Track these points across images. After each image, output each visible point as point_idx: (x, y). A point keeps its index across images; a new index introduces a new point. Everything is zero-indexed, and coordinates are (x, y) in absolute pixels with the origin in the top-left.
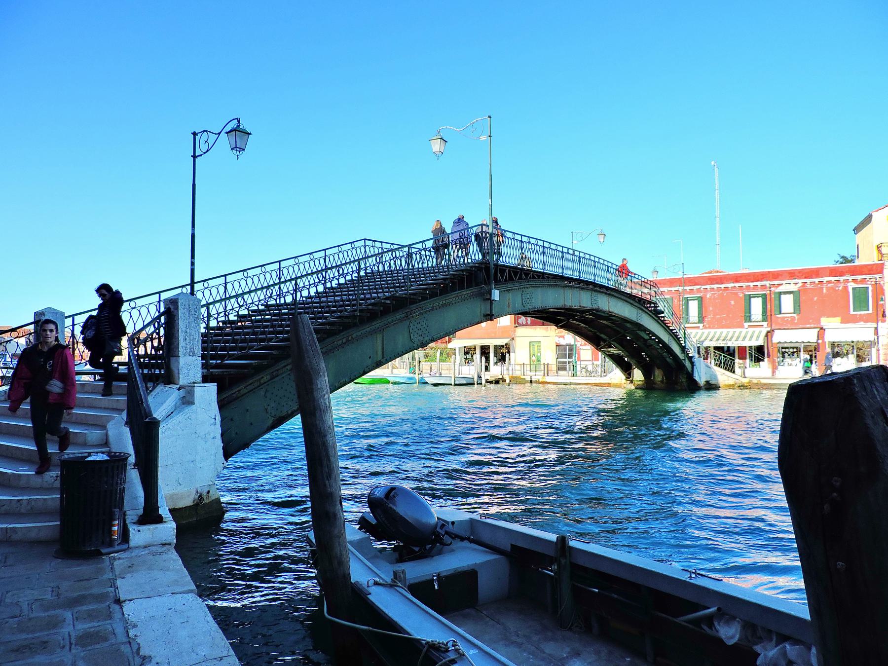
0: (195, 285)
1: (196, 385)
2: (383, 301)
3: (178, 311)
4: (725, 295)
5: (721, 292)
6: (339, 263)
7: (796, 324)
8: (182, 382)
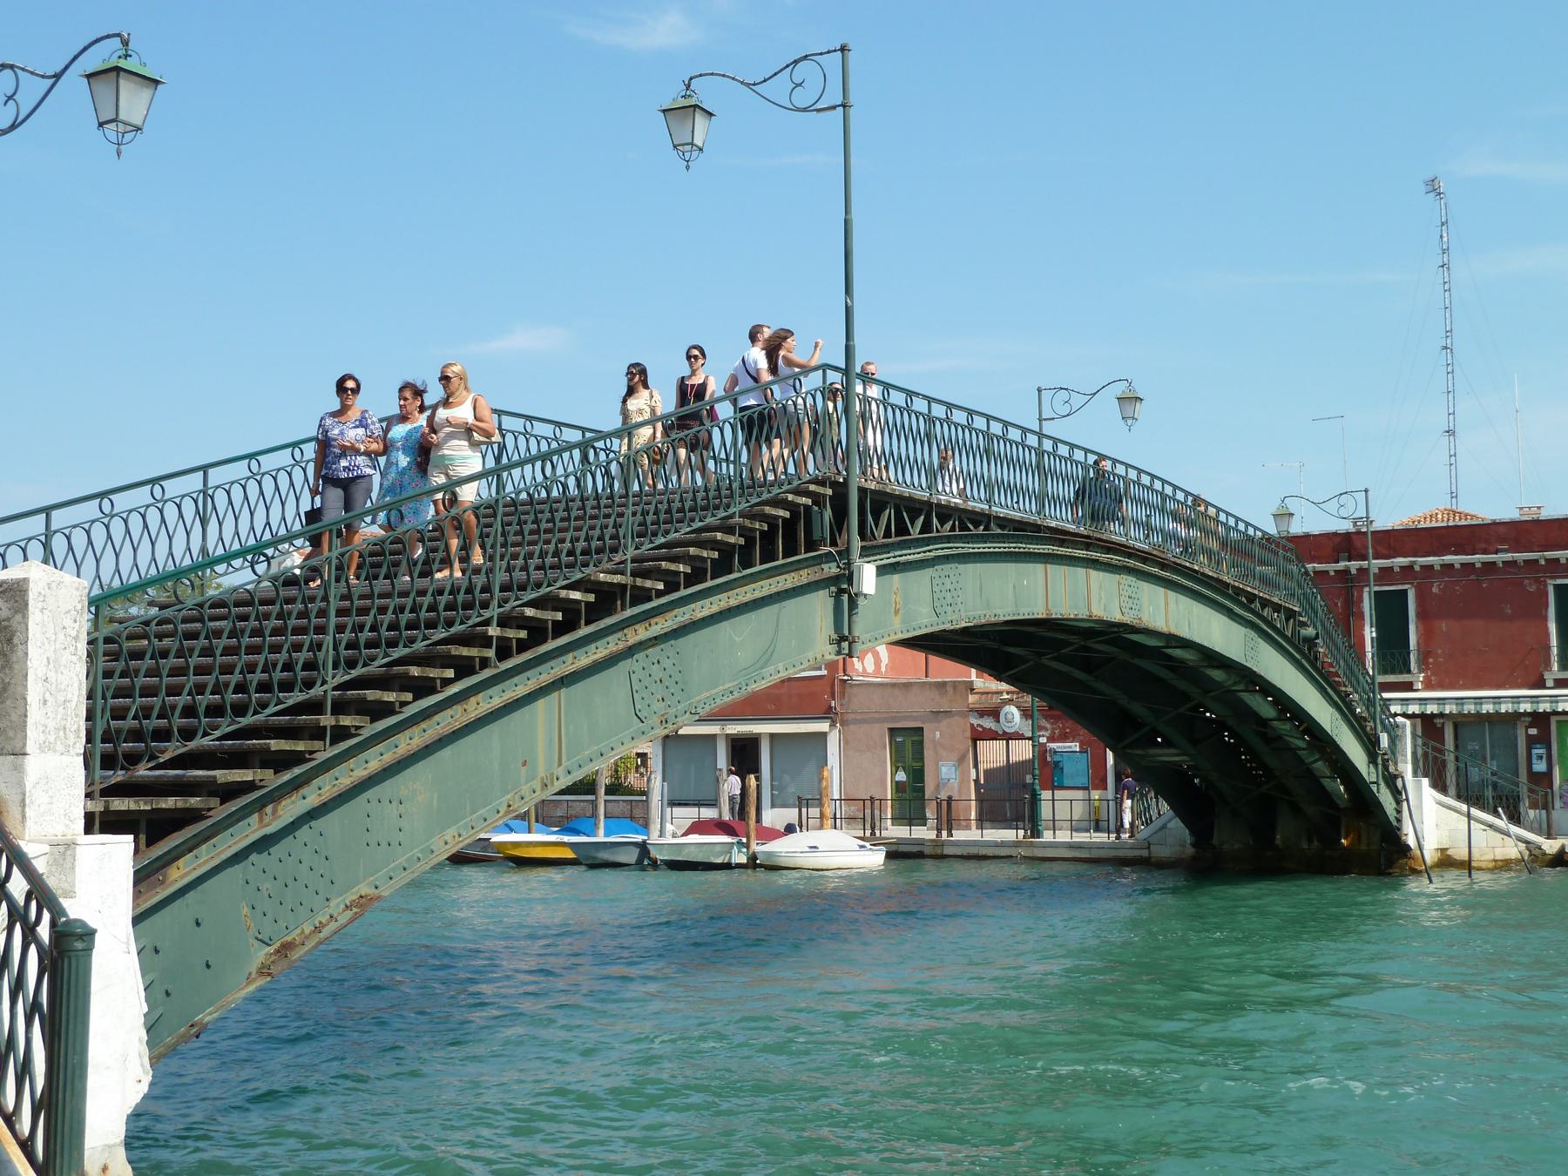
3: (25, 617)
5: (1473, 577)
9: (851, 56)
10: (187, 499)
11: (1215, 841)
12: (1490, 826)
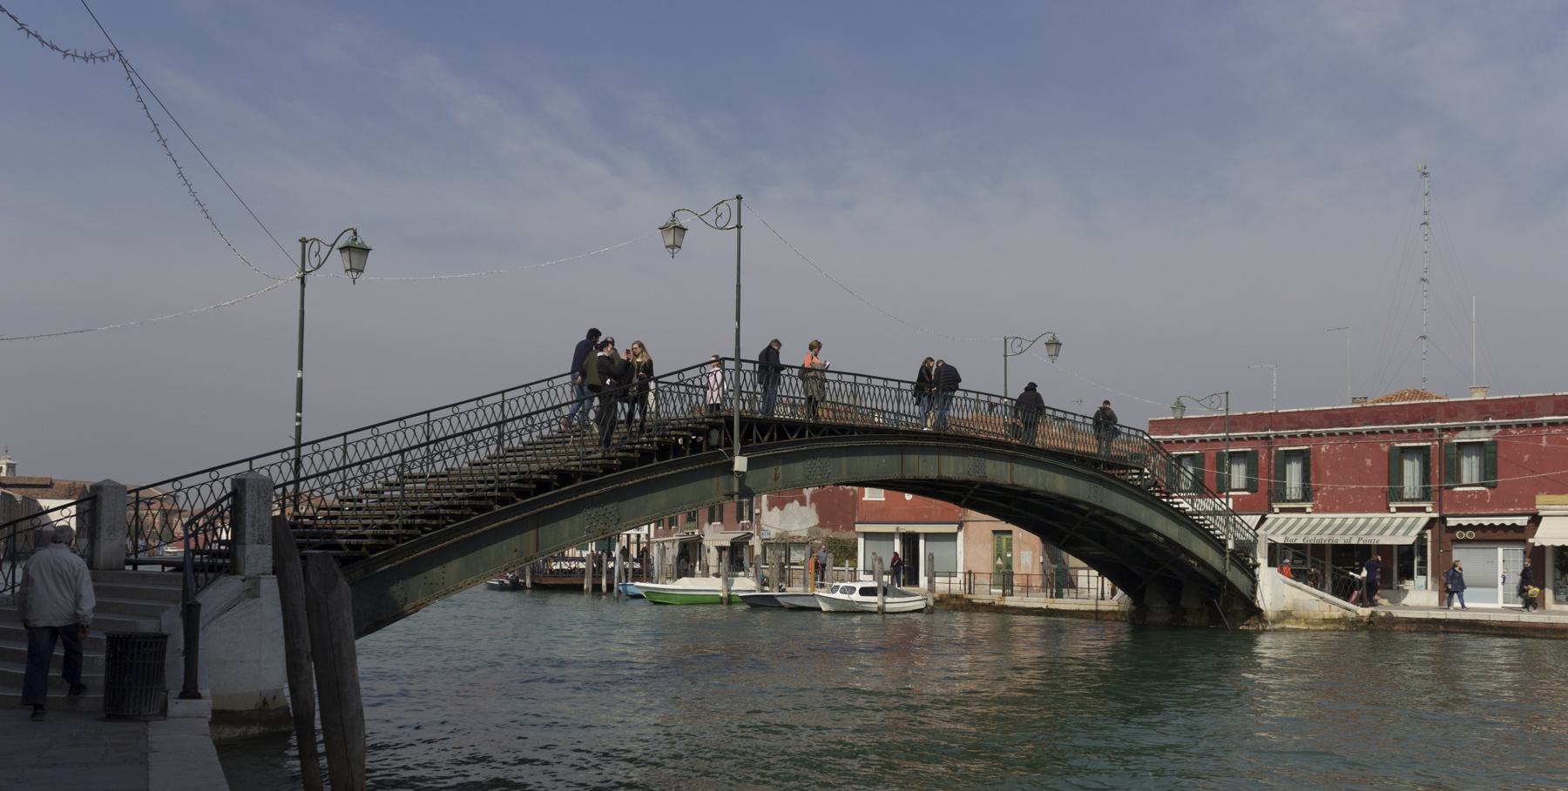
0: (302, 448)
1: (262, 576)
2: (534, 476)
4: (1355, 447)
7: (1487, 506)
8: (248, 572)
10: (389, 435)
11: (1182, 603)
12: (1321, 598)
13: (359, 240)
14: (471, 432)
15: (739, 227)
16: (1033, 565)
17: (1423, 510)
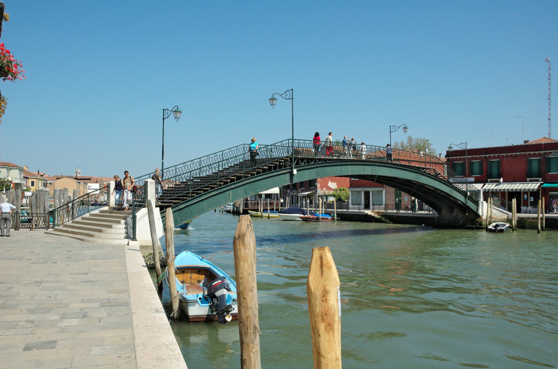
6: (209, 164)
9: (293, 91)
13: (179, 109)
14: (228, 159)
15: (292, 98)
16: (408, 201)
17: (538, 181)
